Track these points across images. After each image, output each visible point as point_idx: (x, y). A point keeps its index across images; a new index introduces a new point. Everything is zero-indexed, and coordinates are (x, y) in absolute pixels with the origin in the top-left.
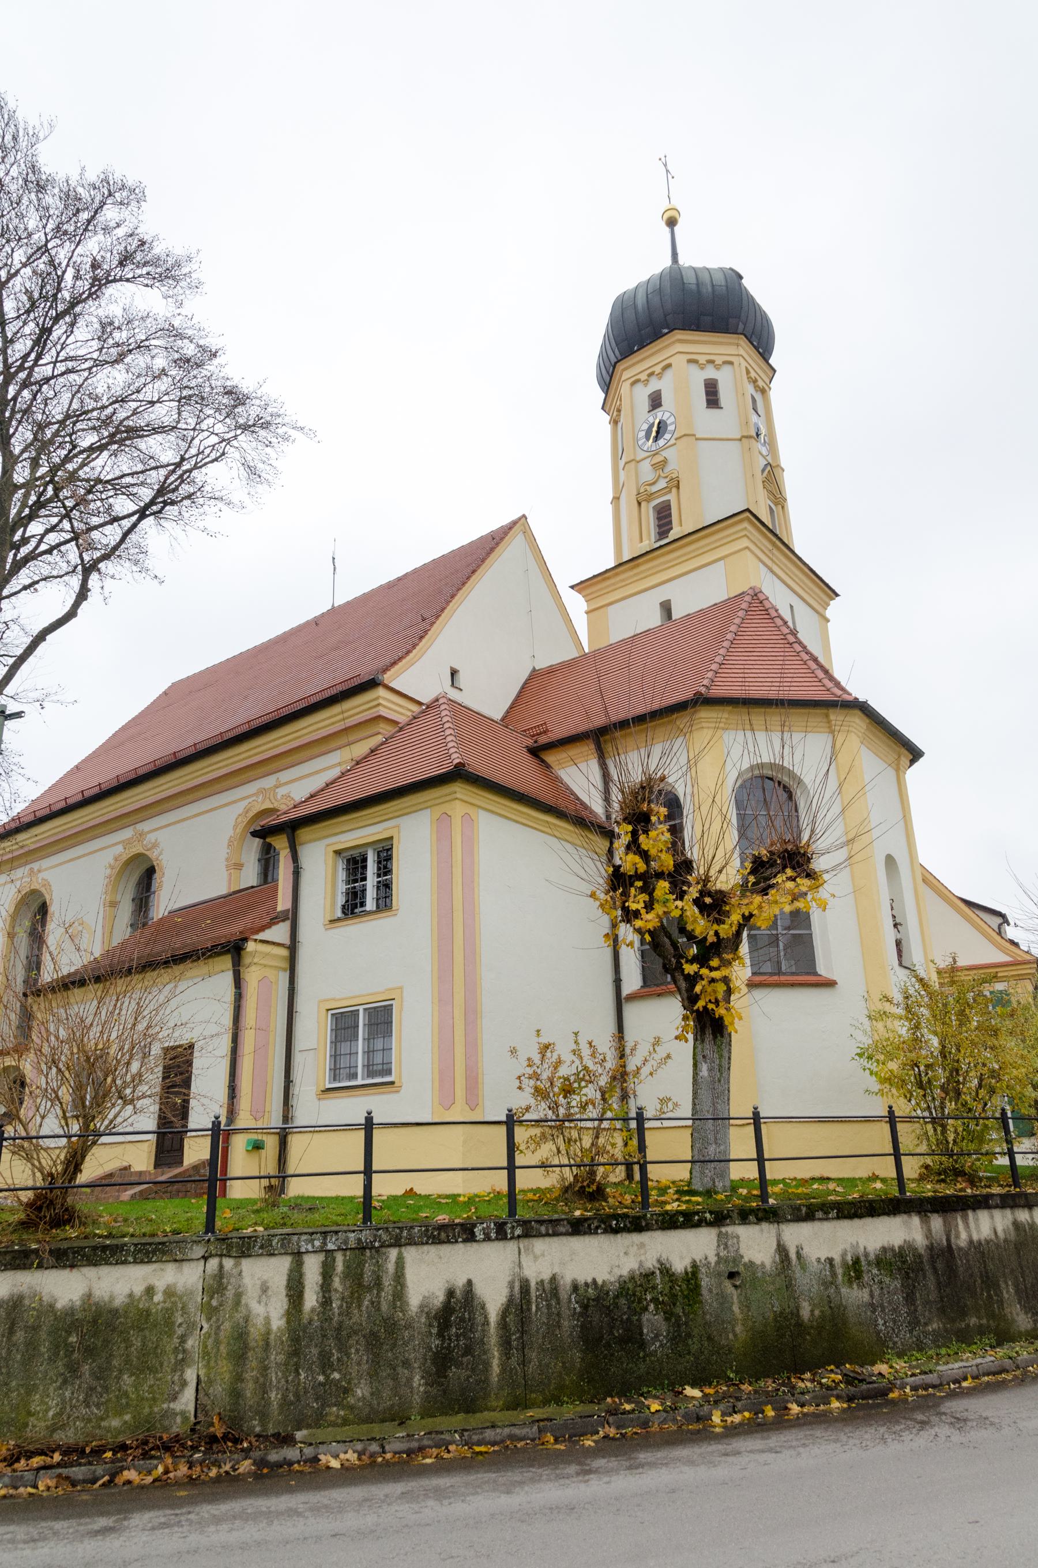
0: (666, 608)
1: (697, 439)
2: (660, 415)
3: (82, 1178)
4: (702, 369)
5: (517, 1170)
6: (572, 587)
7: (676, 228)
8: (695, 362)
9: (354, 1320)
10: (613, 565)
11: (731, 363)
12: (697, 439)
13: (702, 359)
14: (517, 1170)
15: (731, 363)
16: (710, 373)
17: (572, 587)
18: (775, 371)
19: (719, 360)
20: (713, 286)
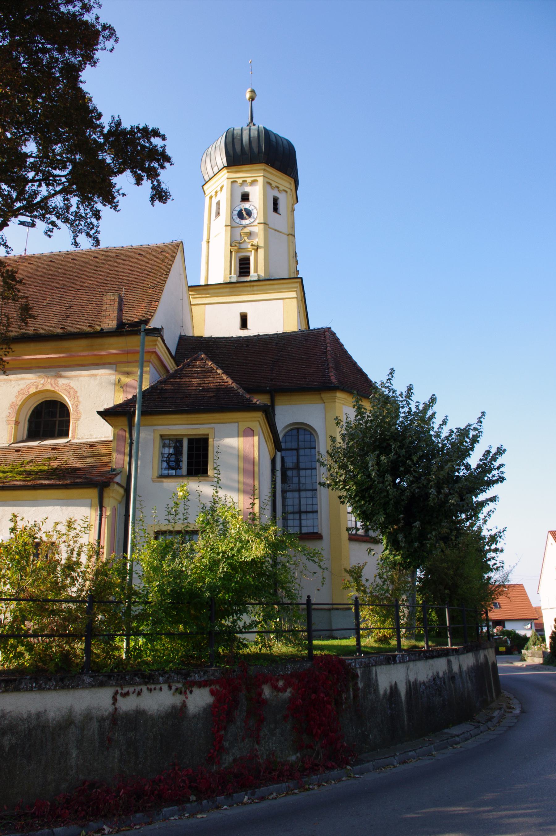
0: (244, 321)
1: (269, 228)
2: (246, 205)
3: (281, 436)
4: (273, 189)
5: (312, 327)
6: (99, 413)
7: (253, 102)
8: (270, 184)
9: (357, 594)
10: (221, 281)
11: (286, 192)
12: (269, 228)
13: (274, 184)
14: (312, 327)
15: (286, 192)
16: (277, 194)
17: (99, 413)
18: (297, 202)
19: (281, 188)
20: (283, 147)
